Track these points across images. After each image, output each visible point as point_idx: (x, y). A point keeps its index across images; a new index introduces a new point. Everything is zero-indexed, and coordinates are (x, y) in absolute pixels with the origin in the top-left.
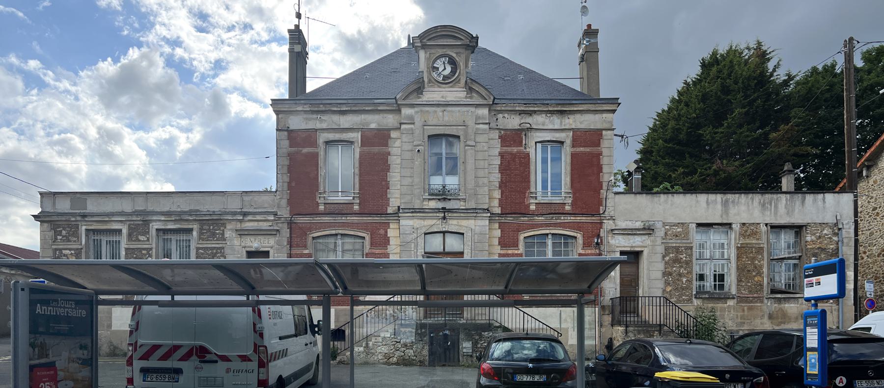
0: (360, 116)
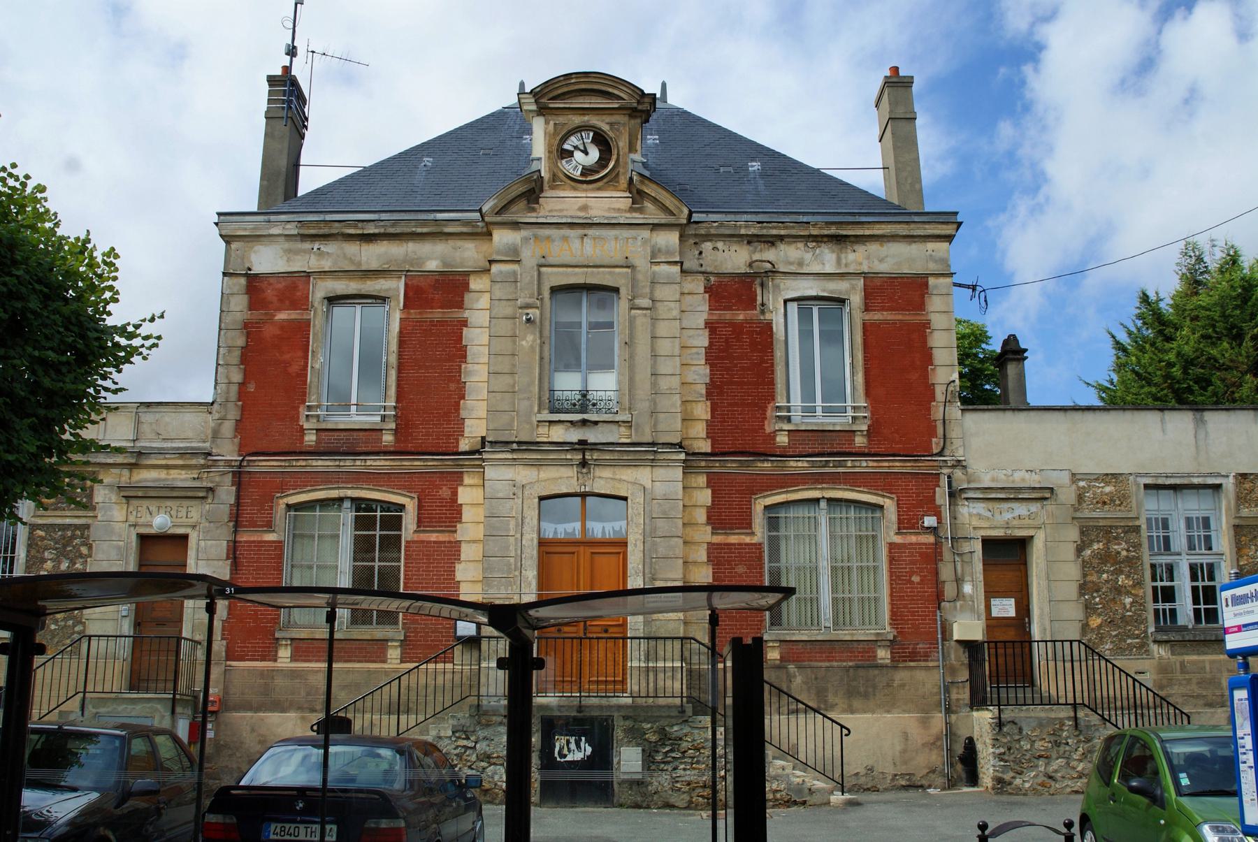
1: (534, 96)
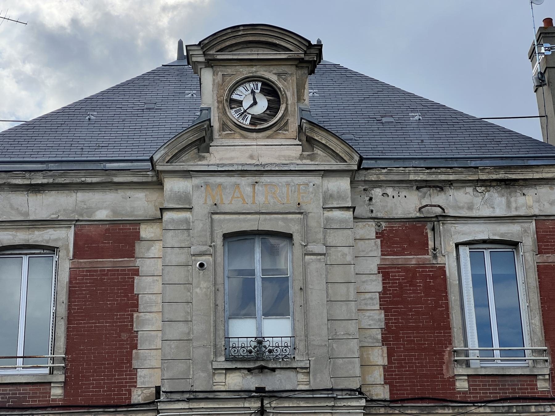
0: (74, 194)
1: (202, 48)
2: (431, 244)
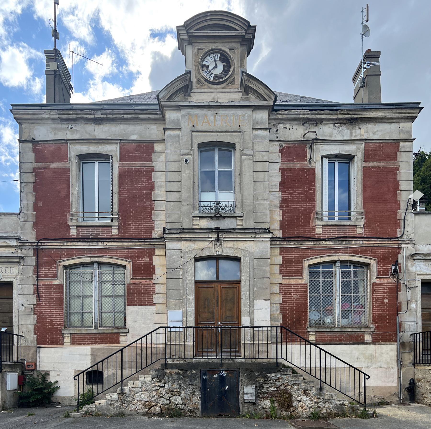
0: (119, 126)
2: (308, 156)
